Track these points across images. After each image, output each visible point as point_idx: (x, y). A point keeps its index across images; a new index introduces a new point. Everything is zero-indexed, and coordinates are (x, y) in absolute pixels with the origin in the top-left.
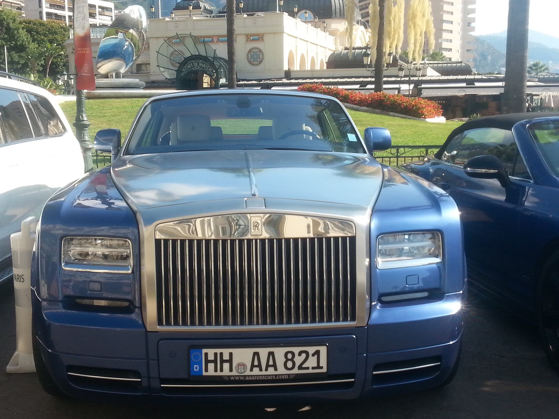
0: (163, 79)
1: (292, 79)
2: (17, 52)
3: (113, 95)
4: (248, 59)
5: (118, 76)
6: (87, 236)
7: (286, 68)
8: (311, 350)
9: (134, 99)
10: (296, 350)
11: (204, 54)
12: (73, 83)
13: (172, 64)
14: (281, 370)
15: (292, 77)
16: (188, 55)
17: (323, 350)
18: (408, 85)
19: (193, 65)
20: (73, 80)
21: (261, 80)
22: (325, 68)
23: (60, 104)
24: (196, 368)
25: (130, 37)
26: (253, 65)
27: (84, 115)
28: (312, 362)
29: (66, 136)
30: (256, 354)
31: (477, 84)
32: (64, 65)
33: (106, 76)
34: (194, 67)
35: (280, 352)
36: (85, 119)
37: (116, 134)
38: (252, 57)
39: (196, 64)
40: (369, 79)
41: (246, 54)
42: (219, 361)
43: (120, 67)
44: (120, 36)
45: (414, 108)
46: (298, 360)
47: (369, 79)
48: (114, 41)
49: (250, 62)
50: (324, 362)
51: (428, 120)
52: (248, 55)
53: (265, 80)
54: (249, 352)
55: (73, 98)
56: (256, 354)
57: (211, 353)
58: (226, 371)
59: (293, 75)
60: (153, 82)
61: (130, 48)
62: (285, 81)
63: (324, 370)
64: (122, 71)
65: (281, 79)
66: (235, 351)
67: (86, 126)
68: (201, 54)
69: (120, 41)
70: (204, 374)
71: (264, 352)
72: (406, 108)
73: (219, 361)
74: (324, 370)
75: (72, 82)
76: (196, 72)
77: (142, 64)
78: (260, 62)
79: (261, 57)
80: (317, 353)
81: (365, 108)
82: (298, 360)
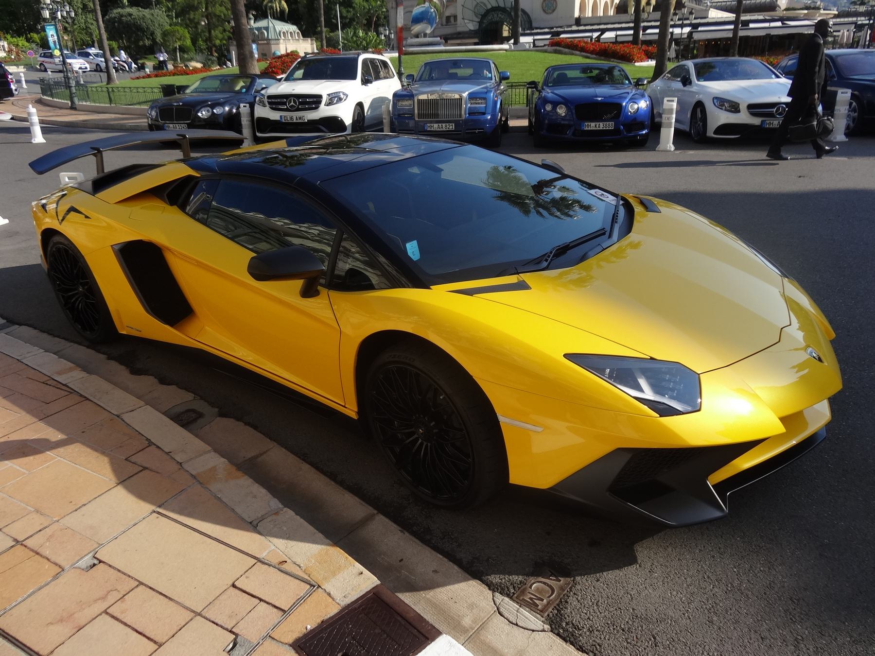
0: (468, 30)
1: (581, 25)
2: (345, 8)
3: (421, 51)
4: (543, 8)
5: (425, 35)
6: (402, 100)
7: (577, 15)
8: (451, 124)
9: (434, 54)
10: (447, 124)
11: (502, 5)
12: (393, 37)
13: (477, 16)
14: (444, 129)
15: (581, 23)
16: (489, 7)
17: (453, 124)
18: (680, 29)
19: (493, 16)
20: (393, 35)
21: (552, 28)
22: (611, 12)
23: (798, 329)
24: (426, 128)
25: (434, 5)
26: (547, 13)
27: (402, 68)
28: (451, 127)
29: (395, 78)
30: (439, 125)
31: (752, 25)
32: (385, 18)
33: (417, 36)
34: (494, 18)
35: (444, 125)
36: (403, 70)
37: (413, 76)
38: (546, 6)
39: (496, 15)
40: (653, 24)
41: (541, 3)
42: (431, 127)
43: (426, 29)
44: (427, 4)
45: (628, 55)
46: (448, 127)
47: (653, 24)
48: (423, 9)
49: (544, 11)
50: (454, 127)
51: (637, 64)
52: (543, 4)
53: (557, 27)
54: (437, 124)
55: (397, 55)
56: (439, 125)
57: (429, 125)
58: (432, 129)
59: (582, 22)
60: (459, 33)
61: (434, 14)
62: (574, 28)
63: (454, 129)
64: (428, 31)
65: (571, 26)
66: (434, 124)
67: (403, 74)
68: (500, 5)
69: (426, 9)
70: (585, 129)
71: (440, 125)
72: (622, 55)
73: (431, 127)
74: (454, 129)
75: (393, 36)
76: (497, 23)
77: (450, 16)
78: (554, 10)
79: (555, 6)
80: (452, 125)
81: (594, 56)
82: (448, 127)
